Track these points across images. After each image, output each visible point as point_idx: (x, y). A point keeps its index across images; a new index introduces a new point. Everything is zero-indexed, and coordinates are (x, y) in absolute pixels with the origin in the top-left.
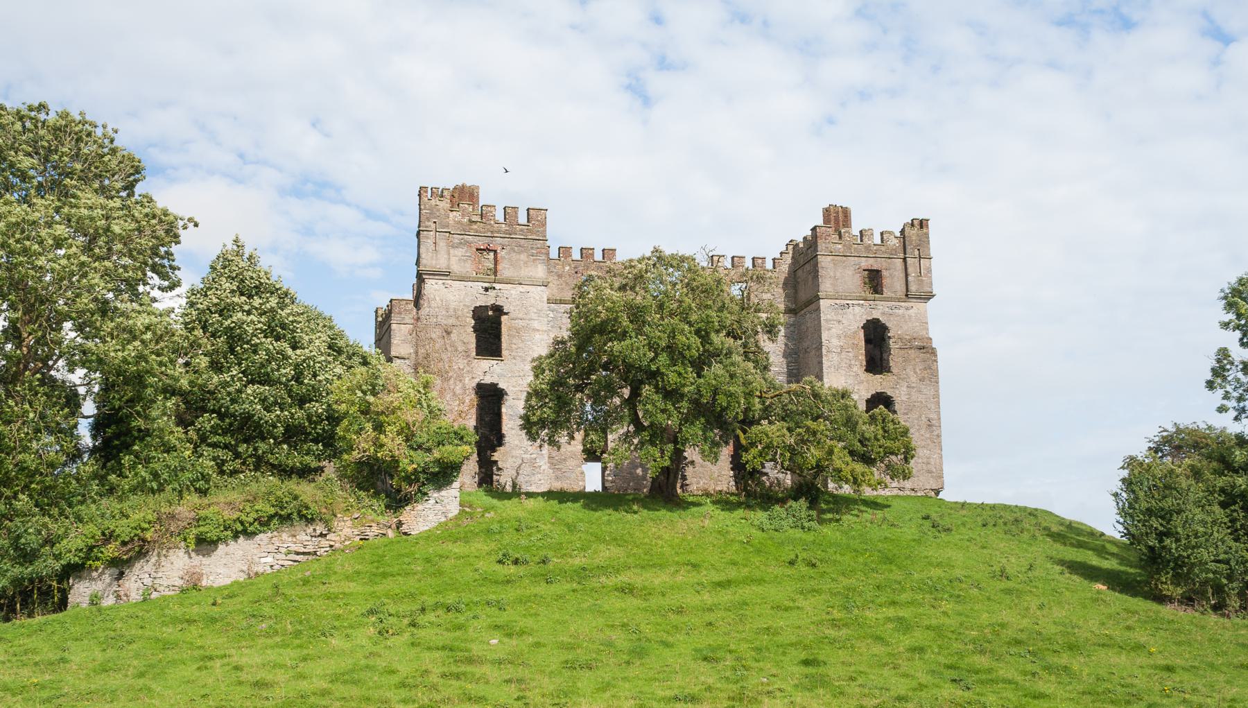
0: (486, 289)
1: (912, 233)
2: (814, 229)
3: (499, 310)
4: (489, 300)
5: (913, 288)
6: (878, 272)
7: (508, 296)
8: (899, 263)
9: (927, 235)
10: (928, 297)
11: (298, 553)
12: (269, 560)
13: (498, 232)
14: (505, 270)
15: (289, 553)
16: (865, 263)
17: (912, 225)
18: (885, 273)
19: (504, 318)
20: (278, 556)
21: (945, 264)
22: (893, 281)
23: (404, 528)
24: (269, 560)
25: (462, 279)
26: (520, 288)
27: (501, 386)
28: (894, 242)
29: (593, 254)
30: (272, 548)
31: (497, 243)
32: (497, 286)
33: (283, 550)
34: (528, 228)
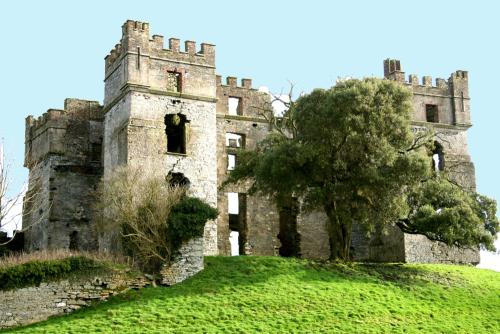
0: (174, 102)
1: (456, 81)
2: (49, 111)
3: (183, 119)
4: (173, 110)
5: (459, 120)
6: (434, 106)
7: (190, 109)
8: (448, 101)
9: (466, 82)
10: (467, 126)
11: (85, 299)
12: (63, 304)
13: (183, 59)
14: (187, 90)
15: (77, 299)
16: (428, 101)
17: (458, 75)
18: (439, 107)
19: (186, 124)
20: (70, 302)
21: (477, 105)
22: (444, 110)
23: (165, 281)
24: (63, 304)
25: (156, 93)
26: (199, 103)
27: (186, 175)
28: (445, 86)
29: (236, 82)
30: (65, 295)
31: (181, 68)
32: (182, 100)
33: (74, 297)
34: (202, 55)
